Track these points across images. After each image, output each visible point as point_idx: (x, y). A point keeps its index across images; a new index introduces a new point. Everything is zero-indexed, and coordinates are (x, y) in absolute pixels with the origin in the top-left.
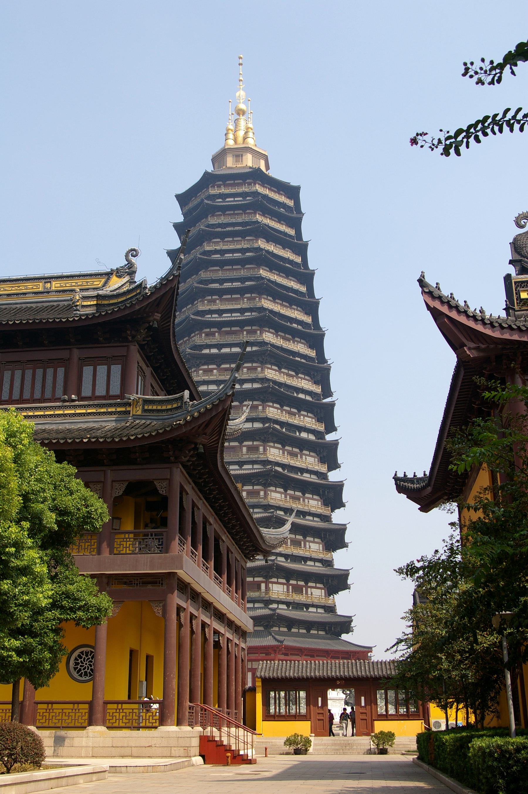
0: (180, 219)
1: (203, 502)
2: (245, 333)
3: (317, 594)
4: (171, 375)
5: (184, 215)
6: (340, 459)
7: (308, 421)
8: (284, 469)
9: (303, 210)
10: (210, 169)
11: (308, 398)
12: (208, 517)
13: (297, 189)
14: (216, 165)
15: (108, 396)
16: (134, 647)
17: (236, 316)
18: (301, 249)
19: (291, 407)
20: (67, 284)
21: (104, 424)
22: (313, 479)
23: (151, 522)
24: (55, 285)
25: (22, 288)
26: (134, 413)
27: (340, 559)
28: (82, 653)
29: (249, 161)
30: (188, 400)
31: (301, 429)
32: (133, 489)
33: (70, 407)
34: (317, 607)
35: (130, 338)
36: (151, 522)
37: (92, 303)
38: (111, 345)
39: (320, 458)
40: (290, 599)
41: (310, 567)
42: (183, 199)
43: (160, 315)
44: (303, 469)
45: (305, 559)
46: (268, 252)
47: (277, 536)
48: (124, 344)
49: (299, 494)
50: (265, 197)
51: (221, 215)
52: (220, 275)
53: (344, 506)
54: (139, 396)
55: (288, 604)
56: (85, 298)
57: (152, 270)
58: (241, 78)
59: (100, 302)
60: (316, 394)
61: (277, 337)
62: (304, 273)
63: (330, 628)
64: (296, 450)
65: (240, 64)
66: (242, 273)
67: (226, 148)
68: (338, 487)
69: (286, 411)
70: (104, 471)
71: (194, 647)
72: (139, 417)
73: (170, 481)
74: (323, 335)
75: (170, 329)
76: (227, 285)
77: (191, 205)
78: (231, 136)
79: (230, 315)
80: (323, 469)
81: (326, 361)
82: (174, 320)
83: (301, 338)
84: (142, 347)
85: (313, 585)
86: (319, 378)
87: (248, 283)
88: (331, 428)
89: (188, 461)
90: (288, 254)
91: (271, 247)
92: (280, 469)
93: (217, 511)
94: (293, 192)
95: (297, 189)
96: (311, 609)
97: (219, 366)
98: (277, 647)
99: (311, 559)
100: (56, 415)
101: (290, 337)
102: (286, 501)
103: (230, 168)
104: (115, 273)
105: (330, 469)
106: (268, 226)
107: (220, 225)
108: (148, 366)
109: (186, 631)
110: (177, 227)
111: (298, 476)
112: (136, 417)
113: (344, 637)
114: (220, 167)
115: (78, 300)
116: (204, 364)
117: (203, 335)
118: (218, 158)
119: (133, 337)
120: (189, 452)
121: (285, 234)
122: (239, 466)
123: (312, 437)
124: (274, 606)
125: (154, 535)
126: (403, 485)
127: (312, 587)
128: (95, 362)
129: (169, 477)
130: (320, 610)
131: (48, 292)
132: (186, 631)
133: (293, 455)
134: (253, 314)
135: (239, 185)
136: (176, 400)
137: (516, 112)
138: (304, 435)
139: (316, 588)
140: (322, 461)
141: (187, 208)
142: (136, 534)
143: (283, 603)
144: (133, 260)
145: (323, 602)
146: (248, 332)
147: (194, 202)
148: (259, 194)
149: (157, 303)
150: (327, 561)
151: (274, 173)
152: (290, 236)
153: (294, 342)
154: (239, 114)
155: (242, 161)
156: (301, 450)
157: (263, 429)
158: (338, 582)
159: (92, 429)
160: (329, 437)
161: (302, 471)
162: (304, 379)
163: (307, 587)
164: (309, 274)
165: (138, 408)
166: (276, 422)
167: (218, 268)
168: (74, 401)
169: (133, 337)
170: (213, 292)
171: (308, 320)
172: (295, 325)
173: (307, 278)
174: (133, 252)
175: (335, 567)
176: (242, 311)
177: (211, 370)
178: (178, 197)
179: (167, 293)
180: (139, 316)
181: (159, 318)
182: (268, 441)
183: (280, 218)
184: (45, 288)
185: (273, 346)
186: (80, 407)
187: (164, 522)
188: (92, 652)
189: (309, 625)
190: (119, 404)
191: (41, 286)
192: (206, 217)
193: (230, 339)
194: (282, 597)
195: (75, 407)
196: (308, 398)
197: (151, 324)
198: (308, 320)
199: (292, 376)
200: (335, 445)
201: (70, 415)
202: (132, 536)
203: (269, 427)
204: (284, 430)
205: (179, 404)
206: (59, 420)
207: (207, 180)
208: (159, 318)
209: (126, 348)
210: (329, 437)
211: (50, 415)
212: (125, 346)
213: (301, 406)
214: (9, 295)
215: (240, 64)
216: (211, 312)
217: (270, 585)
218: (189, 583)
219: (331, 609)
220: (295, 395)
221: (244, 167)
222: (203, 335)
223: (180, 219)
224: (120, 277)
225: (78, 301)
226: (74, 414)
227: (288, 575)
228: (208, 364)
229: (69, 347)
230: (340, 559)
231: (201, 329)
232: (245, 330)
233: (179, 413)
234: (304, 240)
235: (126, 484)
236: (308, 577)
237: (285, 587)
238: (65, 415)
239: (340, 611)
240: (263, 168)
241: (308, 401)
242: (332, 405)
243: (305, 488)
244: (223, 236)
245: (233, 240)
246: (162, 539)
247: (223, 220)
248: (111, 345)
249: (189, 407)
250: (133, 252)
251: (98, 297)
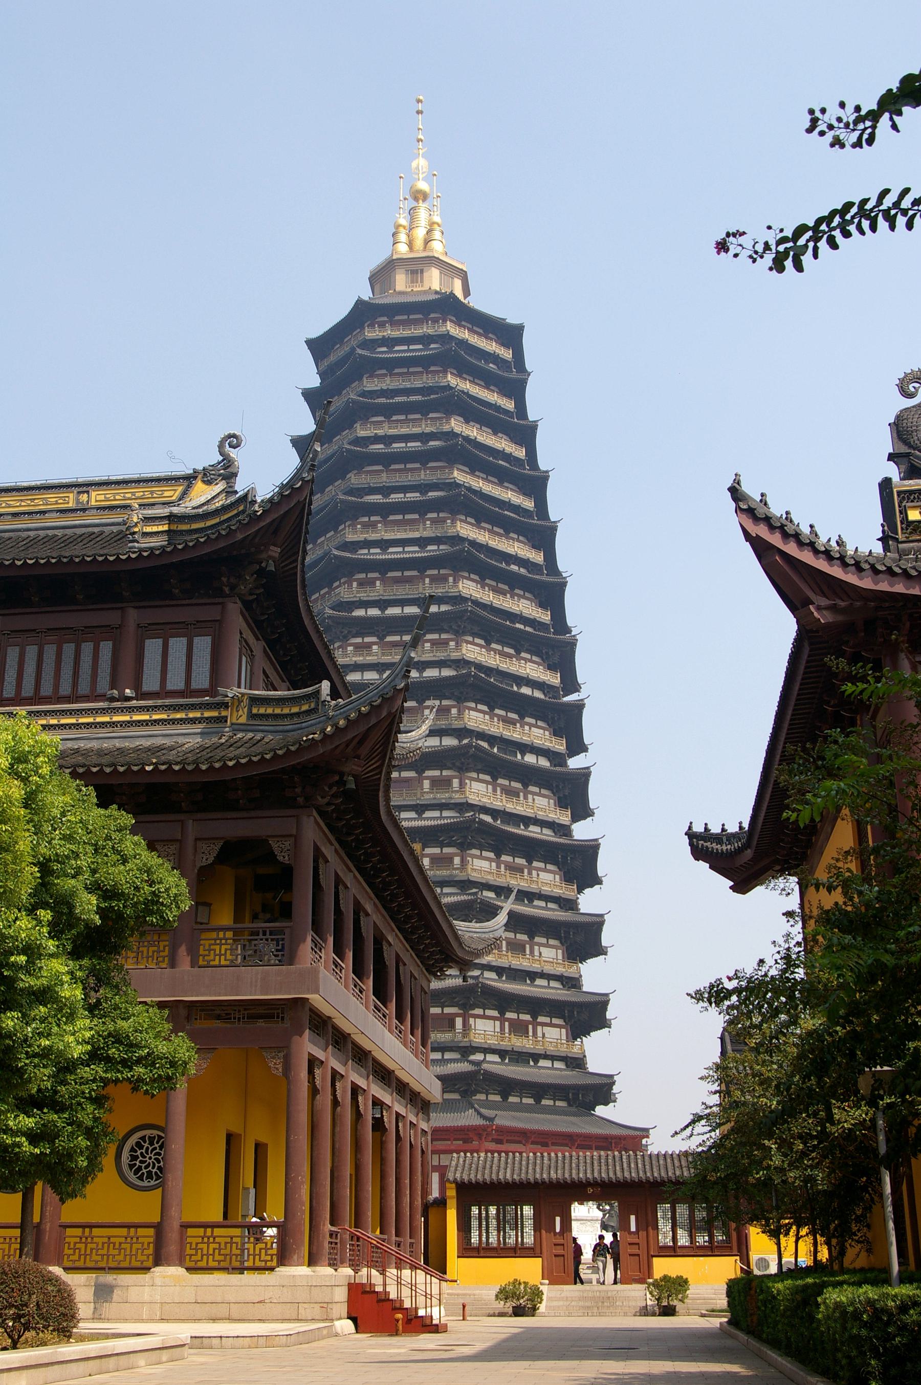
0: (315, 381)
1: (355, 877)
2: (427, 580)
3: (552, 1035)
5: (322, 374)
6: (594, 800)
7: (537, 734)
8: (495, 819)
9: (528, 367)
10: (366, 294)
11: (538, 694)
12: (362, 902)
13: (518, 331)
14: (377, 288)
15: (188, 691)
16: (235, 1129)
17: (412, 552)
18: (525, 434)
19: (507, 709)
20: (117, 496)
21: (181, 740)
22: (547, 835)
23: (264, 911)
24: (96, 497)
25: (39, 502)
26: (234, 721)
27: (594, 975)
28: (143, 1138)
29: (434, 280)
30: (329, 698)
31: (526, 748)
32: (233, 852)
33: (122, 710)
34: (553, 1058)
35: (227, 589)
36: (264, 911)
37: (161, 528)
38: (193, 601)
39: (559, 798)
40: (505, 1044)
41: (541, 989)
42: (319, 347)
43: (279, 550)
44: (529, 818)
45: (532, 976)
46: (467, 439)
47: (483, 936)
48: (217, 600)
49: (521, 861)
50: (463, 343)
51: (385, 375)
52: (384, 479)
53: (600, 882)
54: (243, 690)
55: (502, 1053)
56: (148, 520)
57: (266, 472)
58: (421, 137)
59: (174, 527)
60: (551, 687)
61: (483, 587)
62: (530, 476)
63: (576, 1095)
64: (517, 785)
65: (419, 112)
66: (422, 477)
67: (394, 257)
68: (590, 850)
69: (498, 716)
70: (182, 821)
71: (338, 1129)
72: (242, 727)
73: (296, 838)
74: (564, 584)
75: (296, 574)
76: (396, 497)
77: (333, 358)
78: (403, 237)
79: (400, 549)
80: (564, 818)
81: (569, 631)
82: (304, 559)
83: (525, 590)
84: (247, 605)
85: (546, 1020)
86: (556, 659)
87: (432, 494)
88: (577, 746)
89: (328, 804)
90: (502, 444)
91: (473, 432)
92: (488, 819)
93: (379, 892)
94: (511, 335)
95: (518, 331)
96: (542, 1063)
97: (381, 638)
98: (483, 1128)
99: (542, 975)
100: (98, 723)
101: (506, 587)
102: (499, 875)
103: (401, 293)
104: (200, 476)
105: (576, 818)
106: (467, 394)
107: (383, 393)
108: (258, 639)
109: (325, 1100)
110: (309, 395)
111: (520, 831)
112: (237, 728)
113: (600, 1110)
114: (383, 291)
115: (136, 524)
116: (355, 636)
117: (355, 584)
118: (381, 276)
119: (233, 588)
120: (330, 788)
121: (498, 408)
122: (417, 812)
123: (544, 763)
124: (479, 1057)
125: (268, 933)
126: (703, 846)
127: (544, 1024)
128: (165, 631)
129: (294, 832)
130: (558, 1065)
131: (84, 510)
132: (325, 1100)
133: (510, 793)
134: (441, 547)
135: (416, 322)
136: (307, 697)
137: (900, 195)
138: (530, 759)
139: (551, 1025)
140: (562, 804)
141: (326, 363)
142: (236, 932)
143: (493, 1051)
144: (233, 453)
145: (563, 1050)
146: (433, 579)
147: (339, 353)
148: (452, 338)
149: (275, 529)
150: (570, 979)
151: (477, 302)
152: (506, 412)
153: (512, 597)
154: (416, 199)
155: (422, 281)
156: (525, 785)
157: (459, 748)
158: (589, 1015)
159: (160, 748)
160: (574, 763)
161: (527, 821)
162: (531, 661)
163: (536, 1024)
164: (538, 478)
165: (240, 712)
166: (482, 736)
167: (380, 468)
168: (128, 699)
169: (233, 588)
170: (372, 509)
171: (538, 557)
172: (514, 568)
173: (536, 485)
174: (232, 440)
175: (585, 989)
176: (422, 542)
177: (369, 646)
178: (311, 343)
179: (292, 511)
180: (243, 551)
181: (277, 555)
182: (468, 770)
183: (488, 380)
184: (78, 502)
185: (476, 603)
186: (140, 709)
187: (286, 911)
188: (160, 1137)
189: (539, 1090)
190: (208, 704)
191: (71, 500)
192: (360, 379)
193: (401, 592)
194: (493, 1042)
195: (131, 710)
196: (538, 694)
197: (263, 565)
198: (538, 557)
199: (510, 656)
200: (584, 776)
201: (122, 724)
202: (229, 934)
203: (469, 746)
204: (495, 750)
205: (313, 706)
206: (102, 733)
207: (362, 313)
208: (277, 555)
209: (220, 607)
210: (574, 763)
211: (88, 724)
212: (219, 604)
213: (524, 708)
214: (15, 515)
215: (419, 112)
216: (368, 544)
217: (471, 1020)
218: (329, 1018)
219: (577, 1063)
220: (515, 688)
221: (425, 292)
222: (355, 584)
223: (315, 381)
224: (209, 483)
225: (136, 525)
226: (129, 722)
227: (502, 1002)
228: (362, 635)
229: (120, 605)
230: (594, 975)
231: (351, 574)
232: (428, 576)
233: (312, 720)
234: (531, 419)
235: (220, 844)
236: (537, 1007)
237: (498, 1023)
238: (113, 724)
239: (593, 1066)
240: (459, 293)
241: (538, 699)
242: (579, 707)
243: (533, 851)
244: (388, 412)
245: (407, 419)
246: (283, 939)
247: (389, 383)
248: (193, 601)
249: (330, 710)
250: (232, 440)
251: (171, 518)
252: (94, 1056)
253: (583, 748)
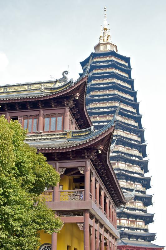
1: (100, 179)
2: (109, 117)
3: (141, 224)
4: (82, 122)
6: (149, 168)
7: (136, 152)
8: (126, 172)
9: (131, 67)
11: (135, 143)
12: (101, 186)
14: (96, 50)
16: (70, 245)
17: (106, 110)
18: (131, 82)
19: (128, 146)
20: (38, 87)
21: (54, 143)
22: (138, 176)
23: (76, 188)
24: (33, 87)
25: (19, 89)
26: (68, 138)
27: (150, 210)
28: (45, 247)
29: (109, 48)
30: (93, 130)
31: (132, 156)
32: (68, 171)
33: (39, 136)
34: (141, 229)
35: (66, 105)
36: (76, 188)
37: (49, 91)
38: (58, 108)
39: (141, 168)
40: (129, 226)
41: (137, 212)
42: (83, 64)
43: (79, 94)
44: (134, 172)
45: (135, 210)
46: (118, 84)
47: (129, 197)
48: (63, 108)
49: (132, 182)
50: (116, 62)
51: (98, 70)
54: (71, 130)
55: (128, 228)
56: (46, 89)
57: (74, 76)
58: (105, 16)
59: (52, 91)
60: (138, 141)
61: (122, 118)
62: (132, 92)
63: (146, 238)
64: (131, 164)
65: (105, 11)
66: (108, 93)
67: (100, 43)
69: (126, 148)
70: (55, 163)
71: (96, 245)
72: (71, 139)
73: (85, 167)
75: (83, 103)
76: (102, 86)
78: (102, 39)
79: (102, 109)
80: (142, 172)
82: (85, 97)
83: (132, 118)
84: (71, 109)
85: (139, 220)
86: (139, 135)
88: (145, 155)
89: (94, 158)
90: (126, 85)
91: (119, 82)
92: (124, 172)
94: (127, 60)
98: (125, 246)
99: (138, 210)
100: (33, 139)
101: (127, 118)
102: (127, 186)
103: (101, 51)
104: (58, 81)
105: (145, 172)
106: (117, 73)
107: (98, 74)
108: (74, 119)
109: (93, 237)
111: (132, 175)
112: (69, 140)
113: (152, 242)
114: (98, 51)
115: (43, 89)
118: (97, 47)
119: (67, 104)
120: (94, 154)
121: (125, 77)
123: (137, 159)
124: (123, 229)
125: (78, 192)
127: (138, 221)
129: (85, 165)
131: (30, 90)
132: (93, 237)
134: (112, 109)
135: (105, 57)
136: (88, 130)
137: (44, 244)
139: (140, 221)
140: (142, 169)
142: (69, 192)
143: (126, 228)
144: (66, 75)
145: (143, 227)
148: (114, 61)
149: (78, 88)
150: (144, 210)
151: (120, 52)
152: (127, 77)
153: (129, 120)
154: (105, 30)
155: (106, 48)
157: (117, 156)
158: (149, 219)
159: (49, 145)
160: (144, 159)
161: (133, 173)
162: (134, 135)
165: (70, 136)
166: (122, 153)
167: (98, 91)
168: (41, 133)
169: (67, 104)
171: (135, 111)
172: (129, 113)
173: (134, 94)
174: (66, 72)
175: (148, 213)
178: (81, 63)
179: (82, 87)
180: (70, 95)
181: (79, 95)
182: (119, 161)
183: (122, 70)
184: (28, 88)
185: (121, 122)
186: (44, 135)
187: (83, 187)
188: (50, 247)
189: (137, 237)
190: (61, 134)
191: (26, 88)
192: (93, 70)
194: (126, 225)
195: (42, 136)
196: (135, 143)
197: (75, 98)
198: (135, 111)
199: (129, 134)
200: (147, 162)
201: (39, 139)
202: (68, 193)
203: (120, 155)
204: (126, 156)
205: (89, 132)
206: (35, 142)
207: (93, 55)
208: (79, 95)
209: (64, 110)
210: (144, 159)
211: (31, 139)
212: (64, 109)
213: (132, 146)
214: (13, 92)
215: (105, 11)
216: (95, 108)
217: (121, 220)
218: (94, 215)
220: (130, 141)
221: (107, 51)
224: (60, 83)
225: (43, 89)
226: (41, 139)
227: (128, 216)
229: (39, 110)
230: (150, 210)
232: (109, 116)
233: (89, 136)
234: (132, 79)
235: (65, 169)
236: (136, 217)
237: (127, 221)
238: (37, 139)
240: (115, 51)
241: (135, 144)
242: (145, 146)
243: (134, 180)
246: (82, 194)
247: (99, 71)
248: (58, 108)
249: (93, 135)
250: (66, 72)
251: (51, 89)
252: (34, 221)
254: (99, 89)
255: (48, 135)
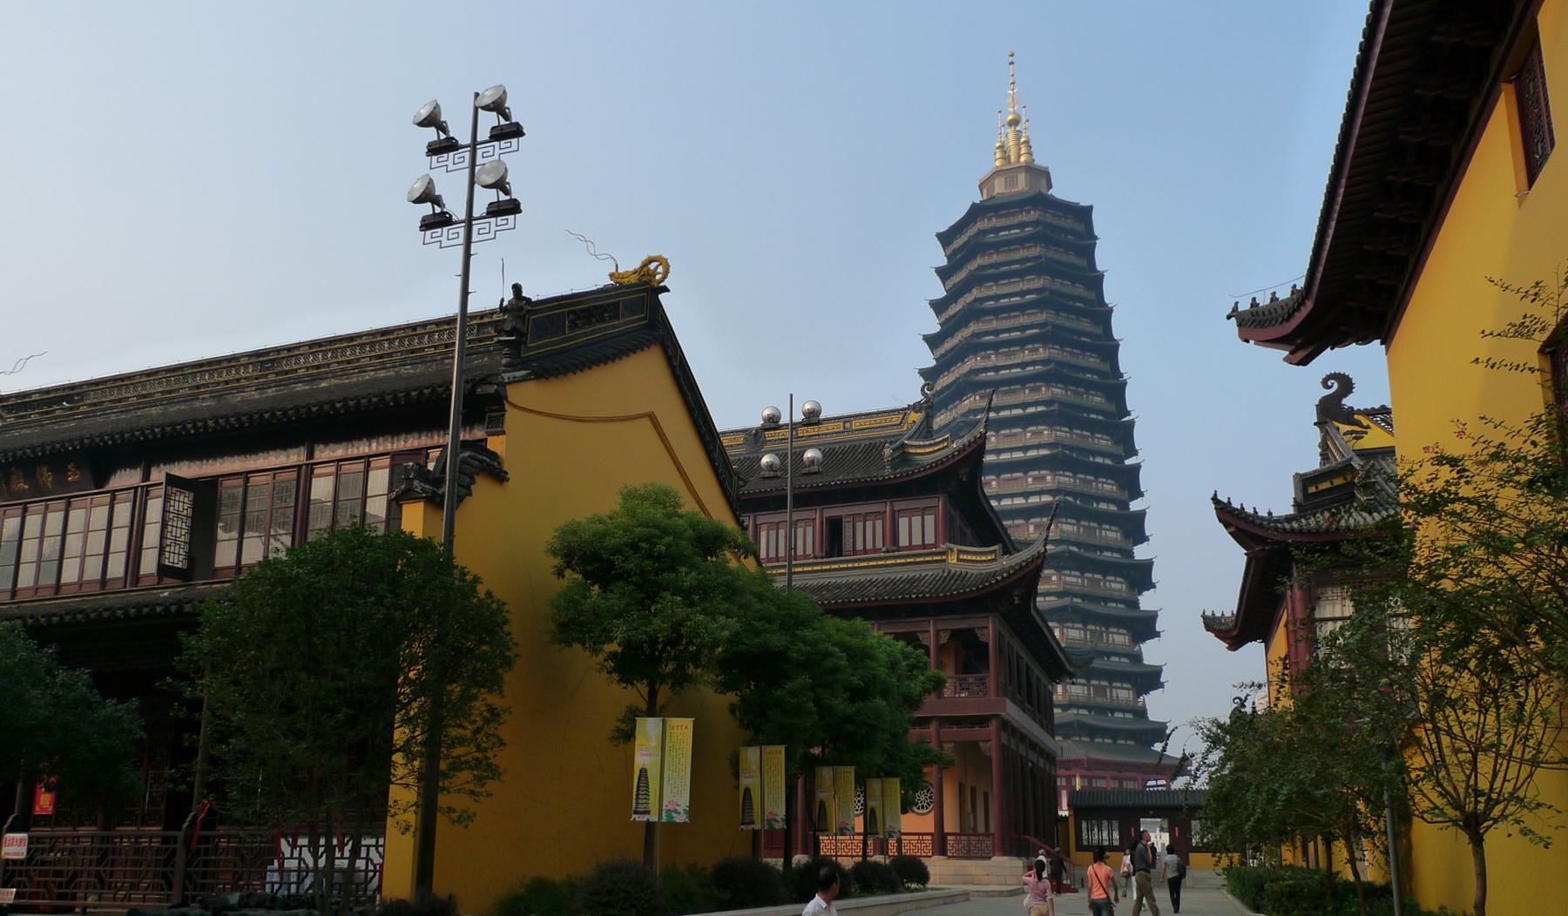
0: (944, 262)
3: (1120, 639)
5: (949, 257)
10: (978, 199)
11: (1108, 462)
15: (924, 546)
24: (856, 424)
31: (1090, 410)
34: (1120, 655)
40: (1078, 489)
42: (945, 238)
52: (994, 325)
53: (1153, 586)
68: (1147, 566)
74: (1125, 383)
76: (1005, 336)
81: (1129, 414)
87: (1030, 332)
92: (1074, 549)
96: (1118, 715)
123: (1113, 508)
126: (1211, 624)
128: (910, 513)
130: (1128, 716)
138: (1103, 506)
141: (945, 316)
146: (1031, 390)
147: (958, 243)
158: (1150, 679)
160: (1135, 506)
163: (1111, 688)
176: (1023, 365)
183: (1069, 248)
189: (1115, 734)
206: (888, 570)
207: (976, 212)
216: (986, 370)
219: (1141, 713)
223: (944, 262)
239: (1153, 716)
244: (996, 278)
253: (1134, 453)
254: (996, 312)
255: (908, 556)
